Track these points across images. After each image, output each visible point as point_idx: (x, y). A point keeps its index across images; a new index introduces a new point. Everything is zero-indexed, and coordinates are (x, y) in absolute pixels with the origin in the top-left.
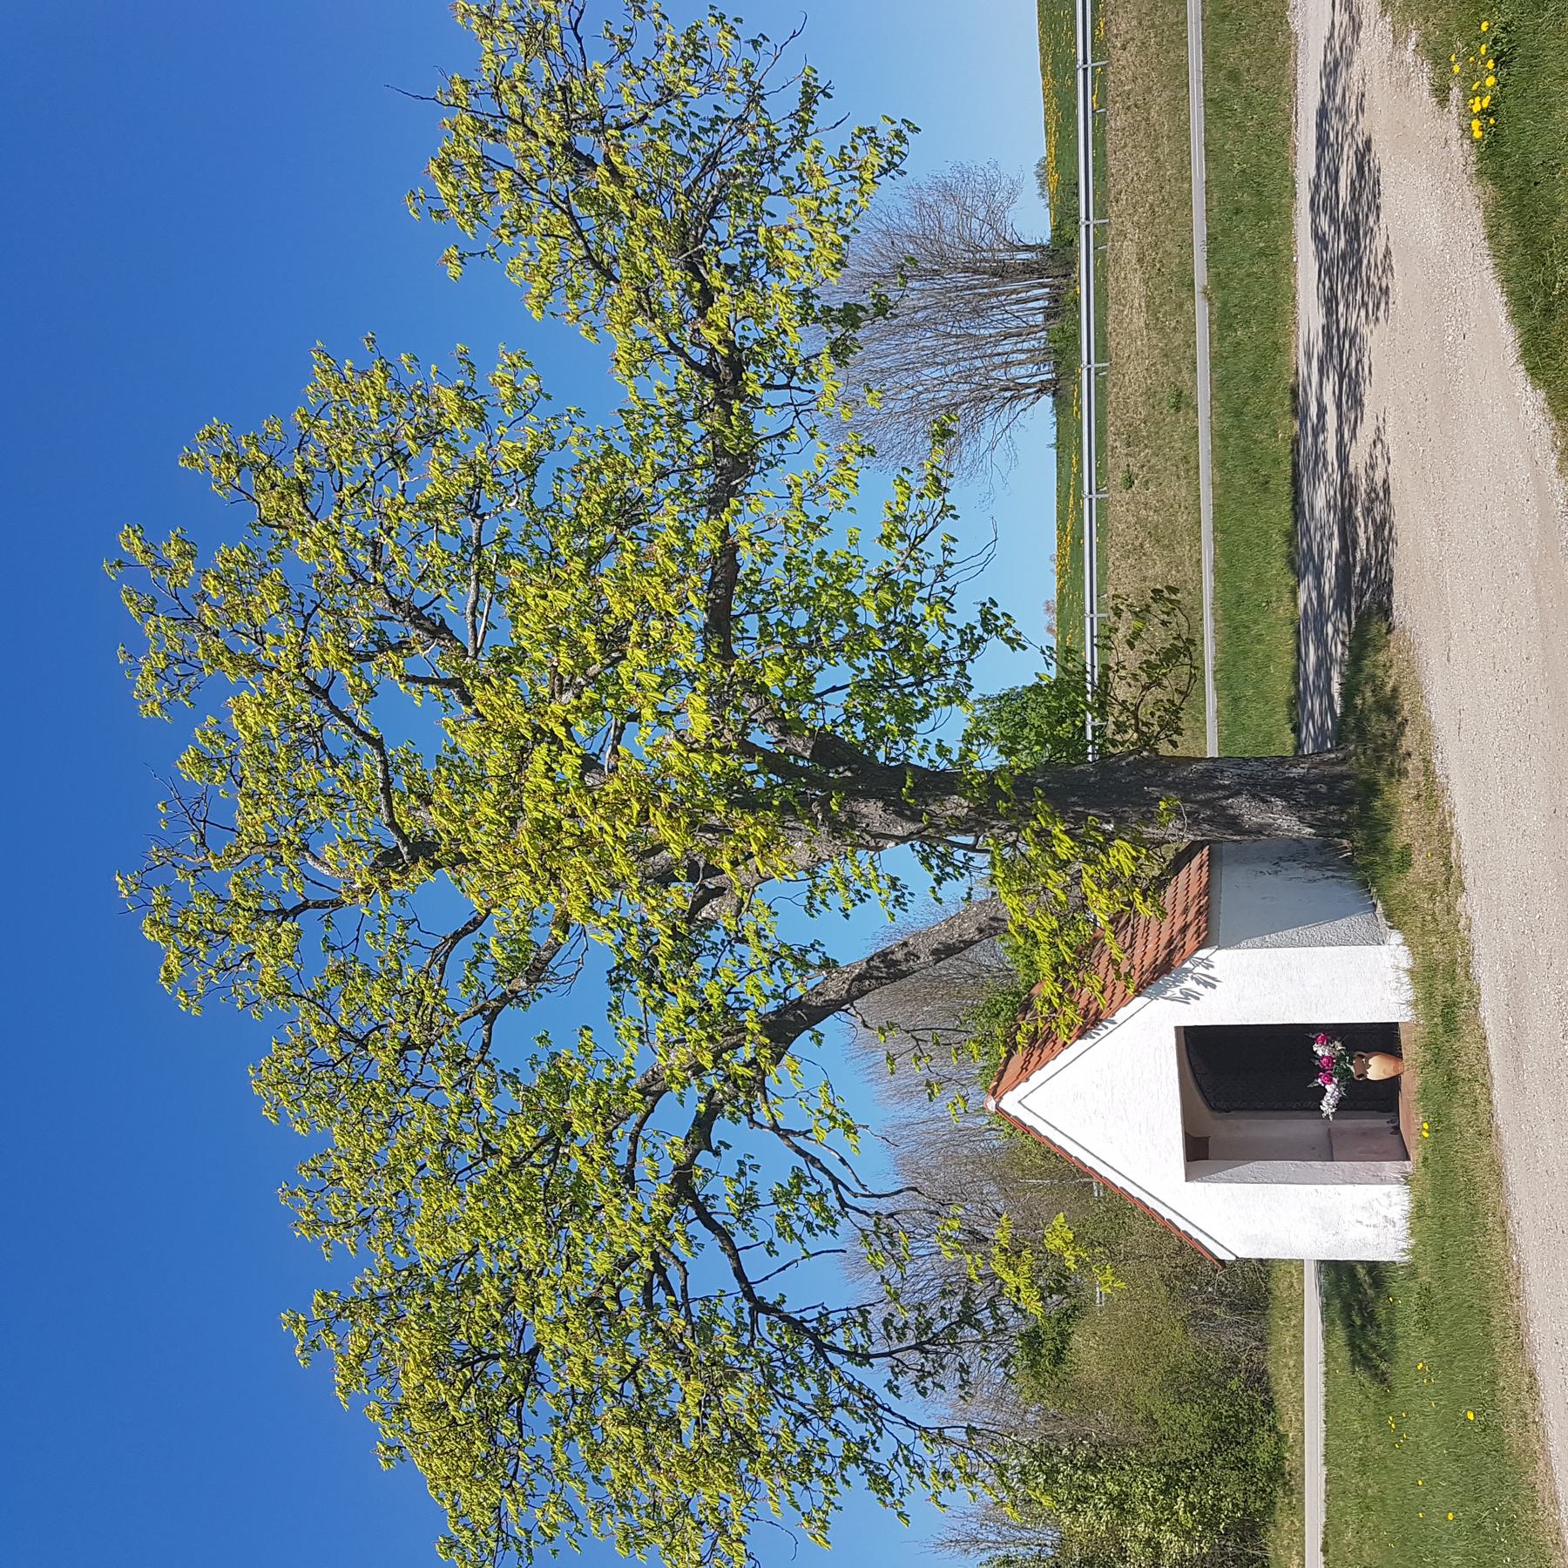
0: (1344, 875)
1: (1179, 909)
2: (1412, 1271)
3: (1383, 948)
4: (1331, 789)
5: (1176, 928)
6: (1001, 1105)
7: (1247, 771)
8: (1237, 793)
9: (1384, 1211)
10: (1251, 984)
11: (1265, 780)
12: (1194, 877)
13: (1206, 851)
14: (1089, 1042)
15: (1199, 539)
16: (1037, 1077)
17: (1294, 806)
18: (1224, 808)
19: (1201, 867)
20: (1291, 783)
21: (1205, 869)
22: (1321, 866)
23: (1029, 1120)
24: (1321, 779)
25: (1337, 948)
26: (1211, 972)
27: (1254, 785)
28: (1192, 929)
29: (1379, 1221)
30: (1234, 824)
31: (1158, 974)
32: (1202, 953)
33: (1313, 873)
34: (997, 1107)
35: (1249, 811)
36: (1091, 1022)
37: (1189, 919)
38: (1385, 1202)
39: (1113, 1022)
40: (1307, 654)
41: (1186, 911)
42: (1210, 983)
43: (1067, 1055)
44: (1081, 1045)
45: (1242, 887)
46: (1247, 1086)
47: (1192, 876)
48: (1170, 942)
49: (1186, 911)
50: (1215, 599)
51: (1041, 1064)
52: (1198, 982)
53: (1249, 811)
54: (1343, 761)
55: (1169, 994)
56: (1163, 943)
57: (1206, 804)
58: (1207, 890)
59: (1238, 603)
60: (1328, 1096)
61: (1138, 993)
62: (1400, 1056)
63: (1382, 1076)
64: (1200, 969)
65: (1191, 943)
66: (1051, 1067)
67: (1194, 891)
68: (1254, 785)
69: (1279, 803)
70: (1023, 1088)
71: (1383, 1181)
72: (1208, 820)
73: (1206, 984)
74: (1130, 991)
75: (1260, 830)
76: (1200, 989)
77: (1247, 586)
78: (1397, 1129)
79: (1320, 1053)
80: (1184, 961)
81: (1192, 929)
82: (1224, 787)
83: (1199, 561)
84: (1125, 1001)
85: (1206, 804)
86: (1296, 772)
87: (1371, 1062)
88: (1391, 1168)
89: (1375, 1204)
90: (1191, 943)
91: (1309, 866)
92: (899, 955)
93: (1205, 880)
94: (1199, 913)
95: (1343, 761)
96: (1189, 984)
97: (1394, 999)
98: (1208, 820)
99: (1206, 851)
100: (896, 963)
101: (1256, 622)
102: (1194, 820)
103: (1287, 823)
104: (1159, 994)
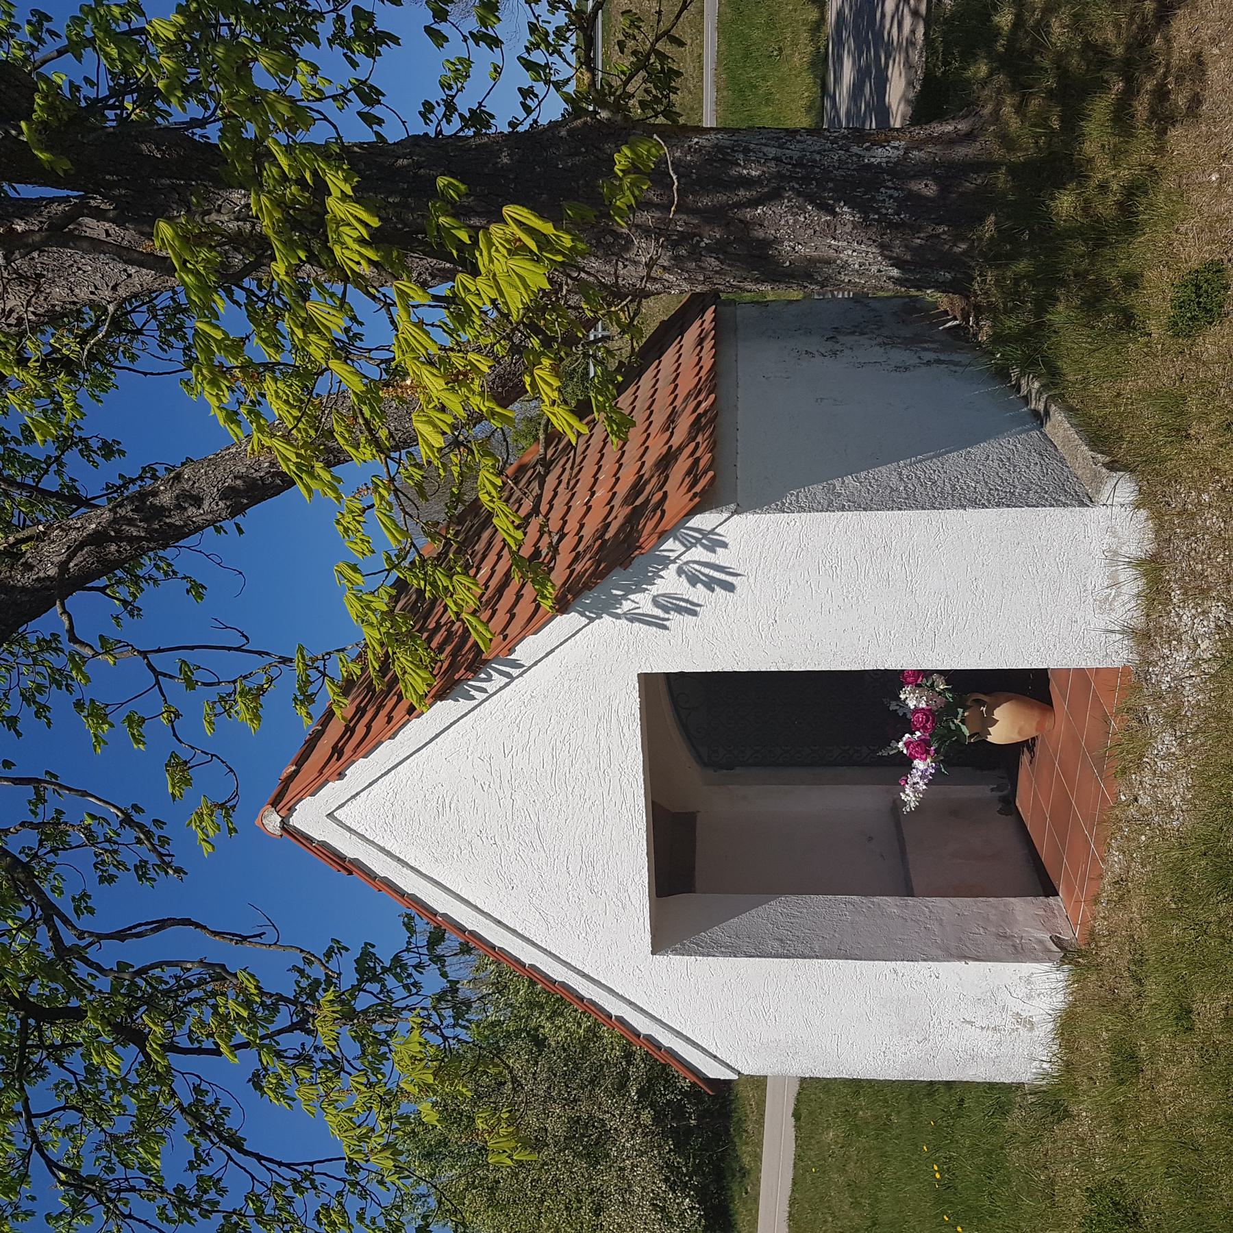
0: (956, 357)
1: (659, 419)
2: (1051, 1102)
3: (1090, 513)
4: (944, 189)
5: (651, 458)
6: (296, 821)
7: (793, 151)
8: (774, 195)
9: (1015, 1006)
10: (805, 584)
11: (828, 170)
12: (689, 359)
13: (709, 315)
14: (464, 705)
15: (701, 32)
16: (360, 770)
17: (875, 223)
18: (746, 225)
19: (701, 341)
20: (873, 177)
21: (708, 344)
22: (910, 342)
23: (349, 848)
24: (923, 171)
25: (991, 513)
26: (721, 557)
27: (806, 180)
28: (682, 464)
29: (1009, 1022)
30: (760, 259)
31: (611, 561)
32: (698, 521)
33: (900, 355)
34: (285, 826)
35: (793, 229)
36: (460, 666)
37: (676, 441)
38: (1021, 991)
39: (515, 664)
40: (838, 79)
41: (672, 419)
42: (719, 581)
43: (416, 730)
44: (445, 709)
45: (779, 386)
46: (776, 785)
47: (687, 357)
48: (637, 488)
49: (672, 419)
50: (719, 62)
51: (366, 747)
52: (693, 580)
53: (793, 229)
54: (970, 136)
55: (627, 606)
56: (623, 489)
57: (714, 216)
58: (713, 381)
59: (747, 55)
60: (915, 777)
61: (562, 606)
62: (1050, 703)
63: (1015, 738)
64: (698, 553)
65: (678, 499)
66: (387, 752)
67: (687, 382)
68: (806, 180)
69: (847, 214)
70: (333, 791)
71: (1019, 953)
72: (718, 249)
73: (710, 584)
74: (546, 605)
75: (806, 272)
76: (698, 593)
77: (756, 34)
78: (1008, 805)
79: (912, 704)
80: (663, 536)
81: (682, 464)
82: (747, 182)
83: (700, 55)
84: (535, 623)
85: (714, 216)
86: (880, 155)
87: (998, 713)
88: (1024, 911)
89: (1003, 995)
90: (678, 499)
91: (890, 342)
92: (166, 499)
93: (707, 363)
94: (696, 427)
95: (970, 136)
96: (669, 582)
97: (1100, 621)
98: (718, 249)
99: (709, 315)
100: (161, 511)
101: (764, 79)
102: (684, 249)
103: (859, 259)
104: (607, 607)
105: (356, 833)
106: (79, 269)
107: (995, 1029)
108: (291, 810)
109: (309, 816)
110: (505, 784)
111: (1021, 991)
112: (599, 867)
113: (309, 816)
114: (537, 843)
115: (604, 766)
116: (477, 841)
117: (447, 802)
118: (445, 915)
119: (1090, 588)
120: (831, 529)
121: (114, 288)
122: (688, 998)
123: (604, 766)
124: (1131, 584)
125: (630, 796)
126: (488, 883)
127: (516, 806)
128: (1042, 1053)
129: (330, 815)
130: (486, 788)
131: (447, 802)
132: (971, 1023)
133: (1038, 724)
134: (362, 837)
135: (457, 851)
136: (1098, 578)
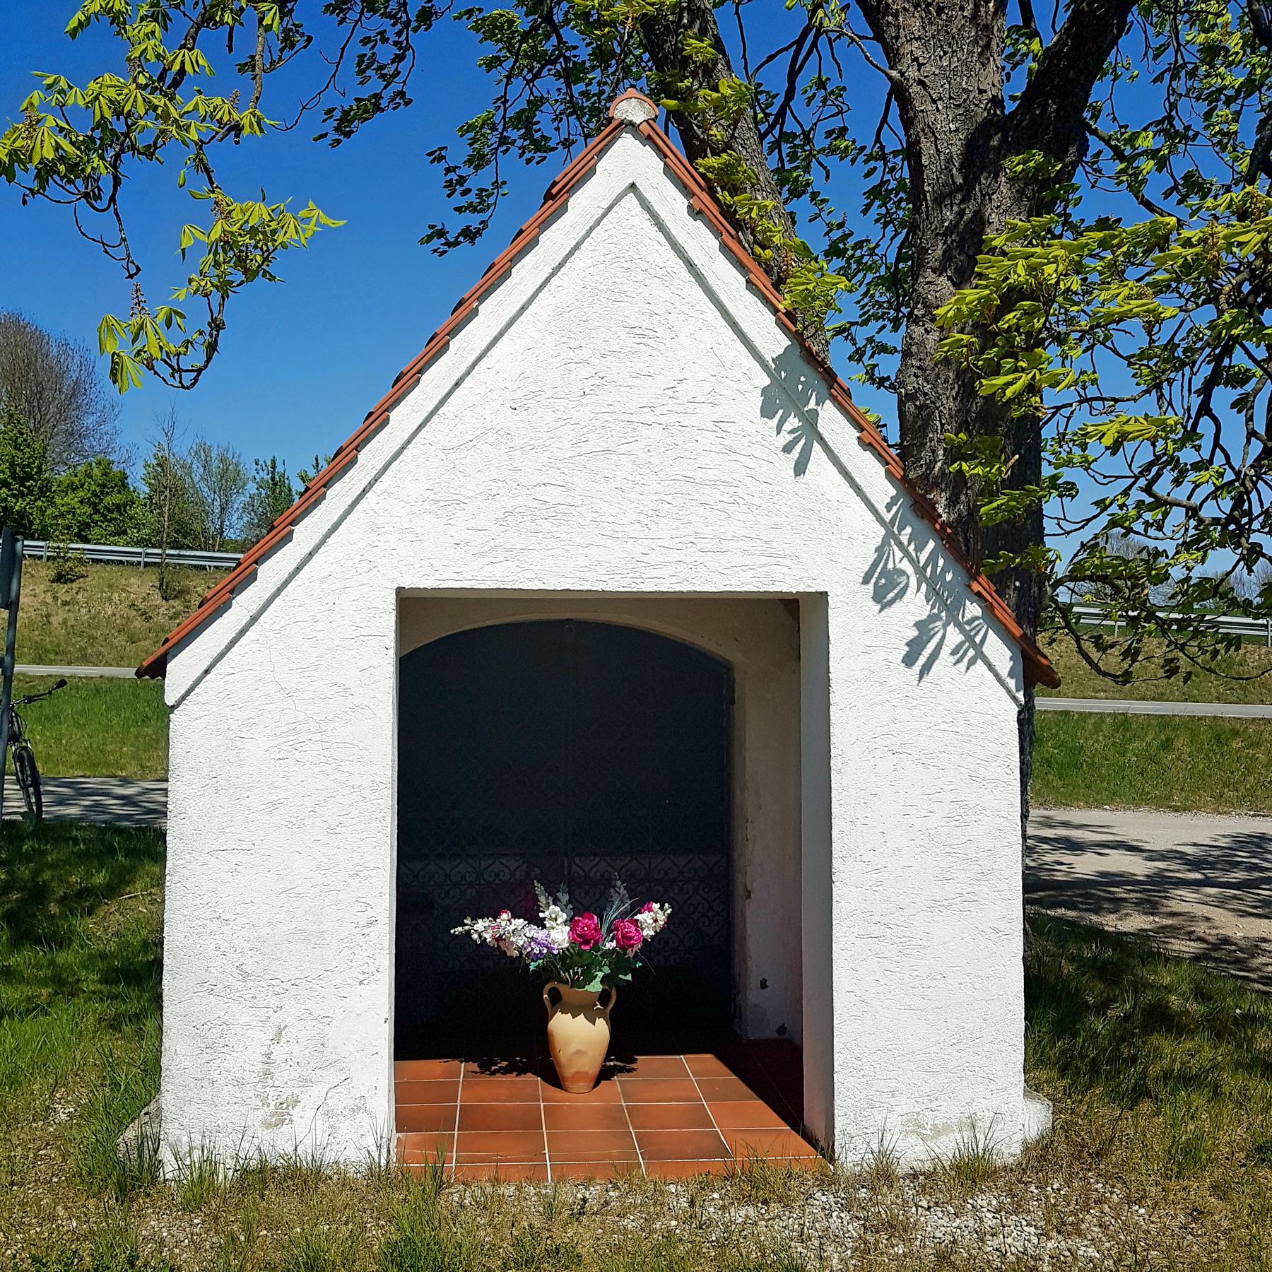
6: (626, 142)
9: (311, 1097)
38: (340, 1101)
89: (331, 1077)
97: (894, 1122)
105: (604, 215)
106: (945, 53)
107: (266, 1073)
108: (648, 140)
109: (629, 161)
110: (675, 418)
111: (340, 1101)
112: (547, 525)
113: (629, 161)
114: (585, 448)
115: (701, 543)
116: (589, 370)
117: (648, 341)
118: (475, 312)
119: (934, 1106)
120: (1003, 814)
121: (921, 83)
122: (320, 636)
123: (701, 543)
124: (948, 1147)
125: (658, 573)
126: (523, 376)
127: (641, 427)
128: (1039, 1106)
129: (633, 186)
130: (669, 392)
131: (648, 341)
132: (277, 1039)
133: (586, 1073)
134: (598, 223)
135: (573, 343)
136: (949, 1111)
